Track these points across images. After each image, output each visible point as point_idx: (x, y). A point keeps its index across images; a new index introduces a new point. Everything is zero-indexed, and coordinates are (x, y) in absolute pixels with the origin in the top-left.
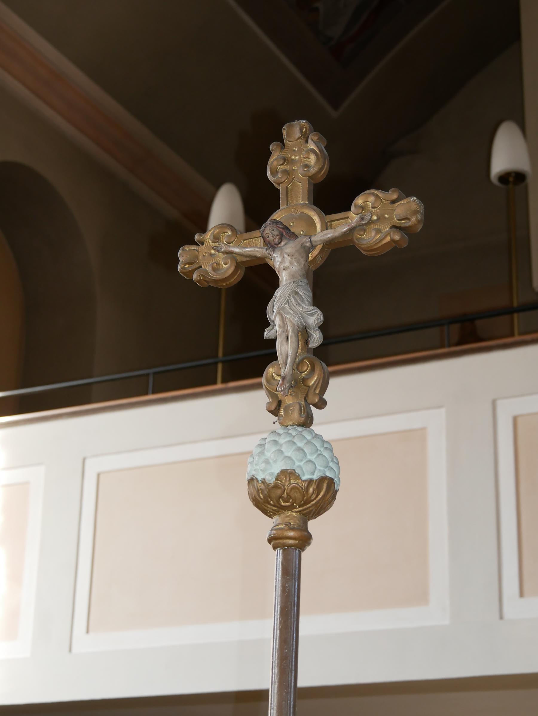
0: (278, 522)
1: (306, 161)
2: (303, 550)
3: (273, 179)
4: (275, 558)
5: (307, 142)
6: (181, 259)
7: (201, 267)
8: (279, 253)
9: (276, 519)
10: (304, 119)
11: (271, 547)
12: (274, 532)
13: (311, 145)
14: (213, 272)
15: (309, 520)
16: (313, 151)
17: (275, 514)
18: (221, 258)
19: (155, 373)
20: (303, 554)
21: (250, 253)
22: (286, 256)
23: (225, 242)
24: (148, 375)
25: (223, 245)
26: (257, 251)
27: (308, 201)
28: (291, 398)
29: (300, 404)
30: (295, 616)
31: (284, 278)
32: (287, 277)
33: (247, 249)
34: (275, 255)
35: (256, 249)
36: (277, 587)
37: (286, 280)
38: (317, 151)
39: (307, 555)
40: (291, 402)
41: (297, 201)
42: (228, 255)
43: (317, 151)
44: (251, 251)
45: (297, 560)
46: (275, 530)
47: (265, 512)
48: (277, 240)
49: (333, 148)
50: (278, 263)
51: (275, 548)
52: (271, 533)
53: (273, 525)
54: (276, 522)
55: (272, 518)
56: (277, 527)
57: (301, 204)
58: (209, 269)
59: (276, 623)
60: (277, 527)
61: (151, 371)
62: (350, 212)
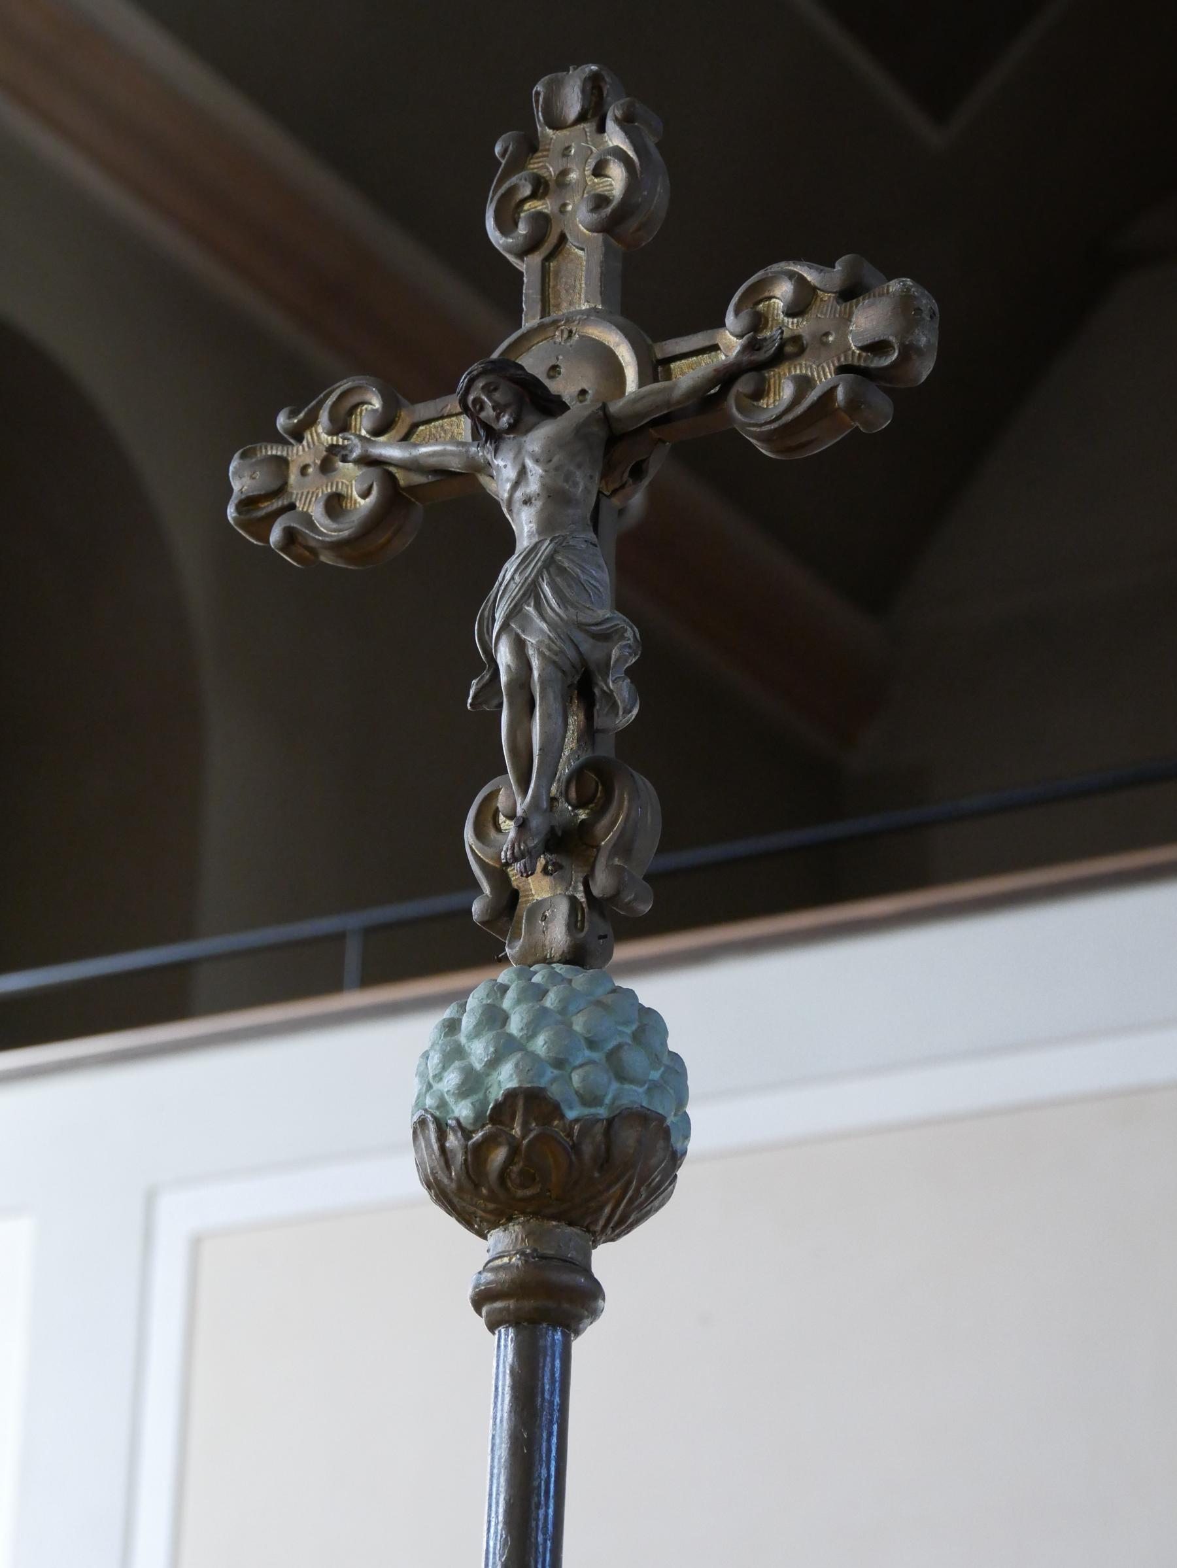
0: (500, 1248)
1: (600, 185)
2: (577, 1333)
3: (502, 240)
4: (490, 1355)
5: (601, 129)
6: (236, 485)
7: (292, 507)
8: (511, 455)
9: (500, 1239)
10: (594, 63)
11: (480, 1322)
12: (489, 1276)
13: (615, 138)
14: (327, 521)
15: (595, 1247)
16: (619, 154)
17: (495, 1226)
18: (350, 478)
19: (369, 932)
20: (579, 1346)
21: (433, 461)
22: (529, 463)
23: (363, 433)
24: (339, 937)
25: (356, 441)
26: (452, 454)
27: (603, 303)
28: (546, 881)
29: (573, 901)
30: (550, 1527)
31: (526, 529)
32: (533, 526)
33: (424, 450)
34: (499, 462)
35: (450, 448)
36: (497, 1441)
37: (531, 535)
38: (631, 154)
39: (591, 1352)
40: (545, 896)
41: (571, 304)
42: (371, 469)
43: (631, 154)
44: (434, 454)
45: (558, 1363)
46: (493, 1270)
47: (466, 1220)
48: (505, 420)
49: (671, 148)
50: (508, 486)
51: (492, 1326)
52: (478, 1279)
53: (487, 1257)
54: (495, 1246)
55: (485, 1237)
56: (498, 1262)
57: (582, 312)
58: (317, 512)
59: (491, 1544)
60: (498, 1262)
61: (353, 921)
62: (721, 330)
